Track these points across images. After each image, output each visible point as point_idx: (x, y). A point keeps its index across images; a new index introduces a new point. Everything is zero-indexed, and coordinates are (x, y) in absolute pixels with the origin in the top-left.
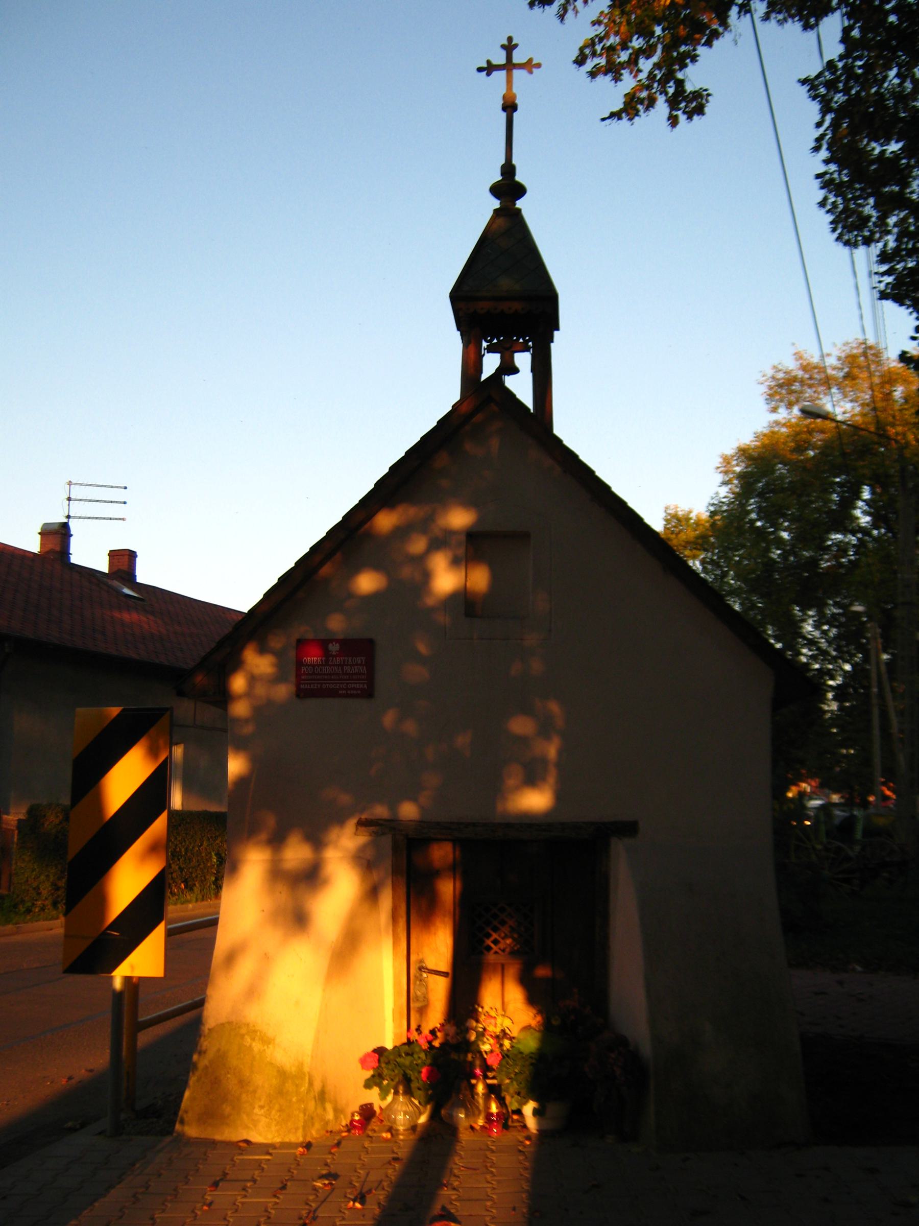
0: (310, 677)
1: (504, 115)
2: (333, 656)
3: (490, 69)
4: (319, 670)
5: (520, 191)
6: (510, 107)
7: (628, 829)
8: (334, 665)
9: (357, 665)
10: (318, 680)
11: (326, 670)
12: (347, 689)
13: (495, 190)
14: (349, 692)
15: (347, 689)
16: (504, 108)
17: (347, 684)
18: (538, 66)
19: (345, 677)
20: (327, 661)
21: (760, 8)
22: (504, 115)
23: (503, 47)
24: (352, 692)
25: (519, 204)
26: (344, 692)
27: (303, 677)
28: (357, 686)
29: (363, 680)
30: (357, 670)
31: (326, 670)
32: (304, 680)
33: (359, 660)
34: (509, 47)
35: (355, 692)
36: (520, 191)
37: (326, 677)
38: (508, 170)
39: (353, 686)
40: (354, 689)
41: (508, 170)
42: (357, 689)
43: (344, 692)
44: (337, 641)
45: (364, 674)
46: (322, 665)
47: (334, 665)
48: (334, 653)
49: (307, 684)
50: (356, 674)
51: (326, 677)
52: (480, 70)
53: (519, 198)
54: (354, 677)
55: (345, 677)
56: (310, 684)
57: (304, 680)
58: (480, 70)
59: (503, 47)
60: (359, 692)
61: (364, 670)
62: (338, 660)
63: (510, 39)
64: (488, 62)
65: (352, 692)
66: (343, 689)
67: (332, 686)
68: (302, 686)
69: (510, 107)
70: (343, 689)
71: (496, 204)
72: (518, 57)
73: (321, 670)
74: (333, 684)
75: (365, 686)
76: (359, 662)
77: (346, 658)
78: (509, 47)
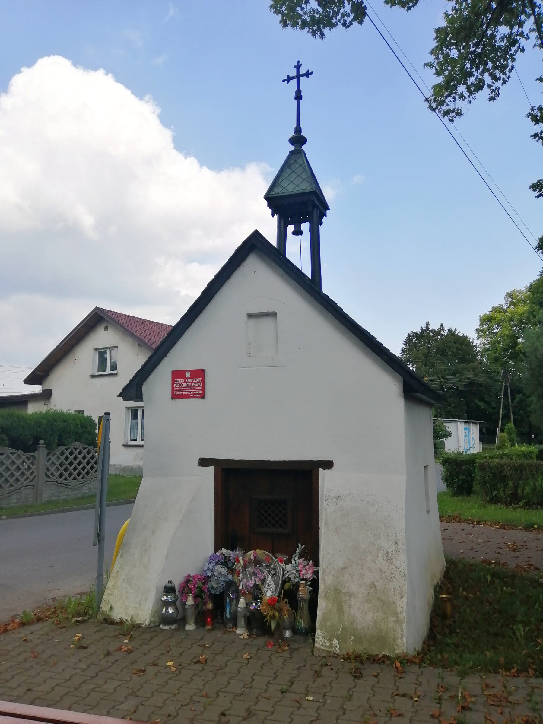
0: (178, 389)
1: (296, 102)
2: (188, 378)
3: (289, 79)
4: (182, 385)
5: (304, 141)
6: (298, 97)
7: (328, 465)
8: (188, 383)
9: (198, 382)
10: (177, 390)
11: (185, 385)
12: (194, 394)
13: (292, 141)
14: (195, 395)
15: (194, 394)
16: (296, 99)
17: (194, 391)
18: (312, 73)
19: (193, 388)
20: (185, 381)
21: (537, 721)
22: (296, 101)
23: (295, 67)
24: (196, 395)
25: (304, 147)
26: (193, 395)
27: (175, 389)
28: (198, 392)
29: (201, 389)
30: (198, 385)
31: (185, 385)
32: (175, 390)
33: (199, 380)
34: (298, 67)
35: (197, 395)
36: (304, 141)
37: (185, 389)
38: (298, 130)
39: (196, 392)
40: (197, 394)
41: (298, 130)
42: (198, 394)
43: (193, 395)
44: (189, 371)
45: (201, 386)
46: (183, 383)
47: (188, 383)
48: (188, 377)
49: (177, 392)
50: (197, 387)
51: (185, 389)
52: (284, 81)
53: (303, 145)
54: (197, 388)
55: (193, 388)
56: (178, 392)
57: (175, 390)
58: (284, 81)
59: (295, 67)
60: (199, 395)
61: (201, 385)
62: (190, 380)
63: (298, 62)
64: (308, 77)
65: (196, 395)
66: (192, 394)
67: (187, 393)
68: (174, 393)
69: (298, 97)
70: (192, 394)
71: (292, 148)
72: (302, 71)
73: (183, 385)
74: (188, 392)
75: (202, 392)
76: (199, 381)
77: (193, 379)
78: (298, 67)
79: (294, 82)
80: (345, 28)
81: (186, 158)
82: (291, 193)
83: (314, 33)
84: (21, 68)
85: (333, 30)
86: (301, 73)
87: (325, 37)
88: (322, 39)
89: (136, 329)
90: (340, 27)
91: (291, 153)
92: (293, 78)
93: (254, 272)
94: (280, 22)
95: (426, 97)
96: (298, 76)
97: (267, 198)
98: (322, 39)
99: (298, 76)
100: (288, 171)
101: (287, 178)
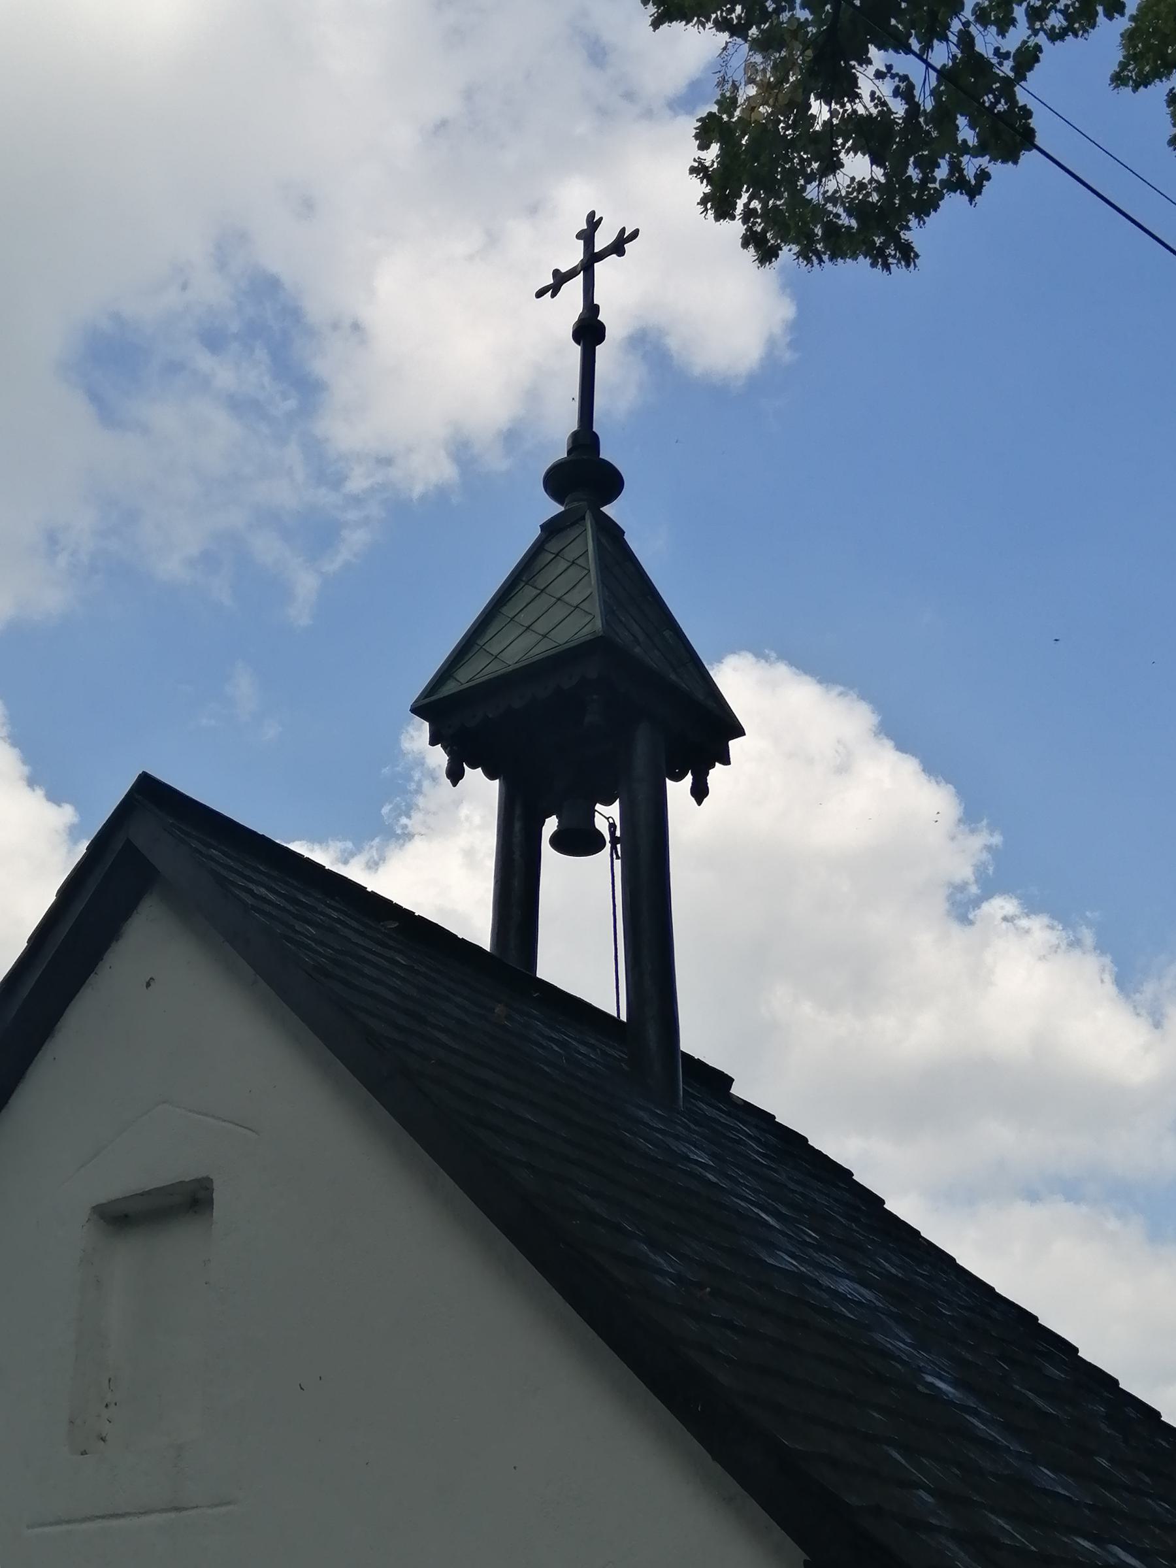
18: (635, 234)
79: (574, 288)
80: (966, 198)
81: (972, 866)
82: (518, 666)
83: (879, 258)
84: (397, 741)
85: (933, 218)
86: (599, 247)
87: (917, 256)
88: (908, 265)
89: (842, 1288)
90: (954, 202)
91: (551, 529)
92: (572, 274)
93: (148, 985)
94: (745, 245)
95: (1035, 151)
96: (591, 259)
97: (416, 708)
98: (908, 265)
99: (591, 259)
100: (529, 592)
101: (516, 619)
